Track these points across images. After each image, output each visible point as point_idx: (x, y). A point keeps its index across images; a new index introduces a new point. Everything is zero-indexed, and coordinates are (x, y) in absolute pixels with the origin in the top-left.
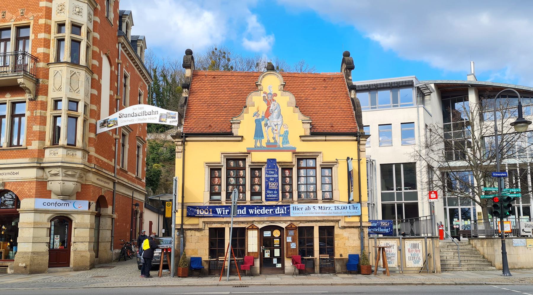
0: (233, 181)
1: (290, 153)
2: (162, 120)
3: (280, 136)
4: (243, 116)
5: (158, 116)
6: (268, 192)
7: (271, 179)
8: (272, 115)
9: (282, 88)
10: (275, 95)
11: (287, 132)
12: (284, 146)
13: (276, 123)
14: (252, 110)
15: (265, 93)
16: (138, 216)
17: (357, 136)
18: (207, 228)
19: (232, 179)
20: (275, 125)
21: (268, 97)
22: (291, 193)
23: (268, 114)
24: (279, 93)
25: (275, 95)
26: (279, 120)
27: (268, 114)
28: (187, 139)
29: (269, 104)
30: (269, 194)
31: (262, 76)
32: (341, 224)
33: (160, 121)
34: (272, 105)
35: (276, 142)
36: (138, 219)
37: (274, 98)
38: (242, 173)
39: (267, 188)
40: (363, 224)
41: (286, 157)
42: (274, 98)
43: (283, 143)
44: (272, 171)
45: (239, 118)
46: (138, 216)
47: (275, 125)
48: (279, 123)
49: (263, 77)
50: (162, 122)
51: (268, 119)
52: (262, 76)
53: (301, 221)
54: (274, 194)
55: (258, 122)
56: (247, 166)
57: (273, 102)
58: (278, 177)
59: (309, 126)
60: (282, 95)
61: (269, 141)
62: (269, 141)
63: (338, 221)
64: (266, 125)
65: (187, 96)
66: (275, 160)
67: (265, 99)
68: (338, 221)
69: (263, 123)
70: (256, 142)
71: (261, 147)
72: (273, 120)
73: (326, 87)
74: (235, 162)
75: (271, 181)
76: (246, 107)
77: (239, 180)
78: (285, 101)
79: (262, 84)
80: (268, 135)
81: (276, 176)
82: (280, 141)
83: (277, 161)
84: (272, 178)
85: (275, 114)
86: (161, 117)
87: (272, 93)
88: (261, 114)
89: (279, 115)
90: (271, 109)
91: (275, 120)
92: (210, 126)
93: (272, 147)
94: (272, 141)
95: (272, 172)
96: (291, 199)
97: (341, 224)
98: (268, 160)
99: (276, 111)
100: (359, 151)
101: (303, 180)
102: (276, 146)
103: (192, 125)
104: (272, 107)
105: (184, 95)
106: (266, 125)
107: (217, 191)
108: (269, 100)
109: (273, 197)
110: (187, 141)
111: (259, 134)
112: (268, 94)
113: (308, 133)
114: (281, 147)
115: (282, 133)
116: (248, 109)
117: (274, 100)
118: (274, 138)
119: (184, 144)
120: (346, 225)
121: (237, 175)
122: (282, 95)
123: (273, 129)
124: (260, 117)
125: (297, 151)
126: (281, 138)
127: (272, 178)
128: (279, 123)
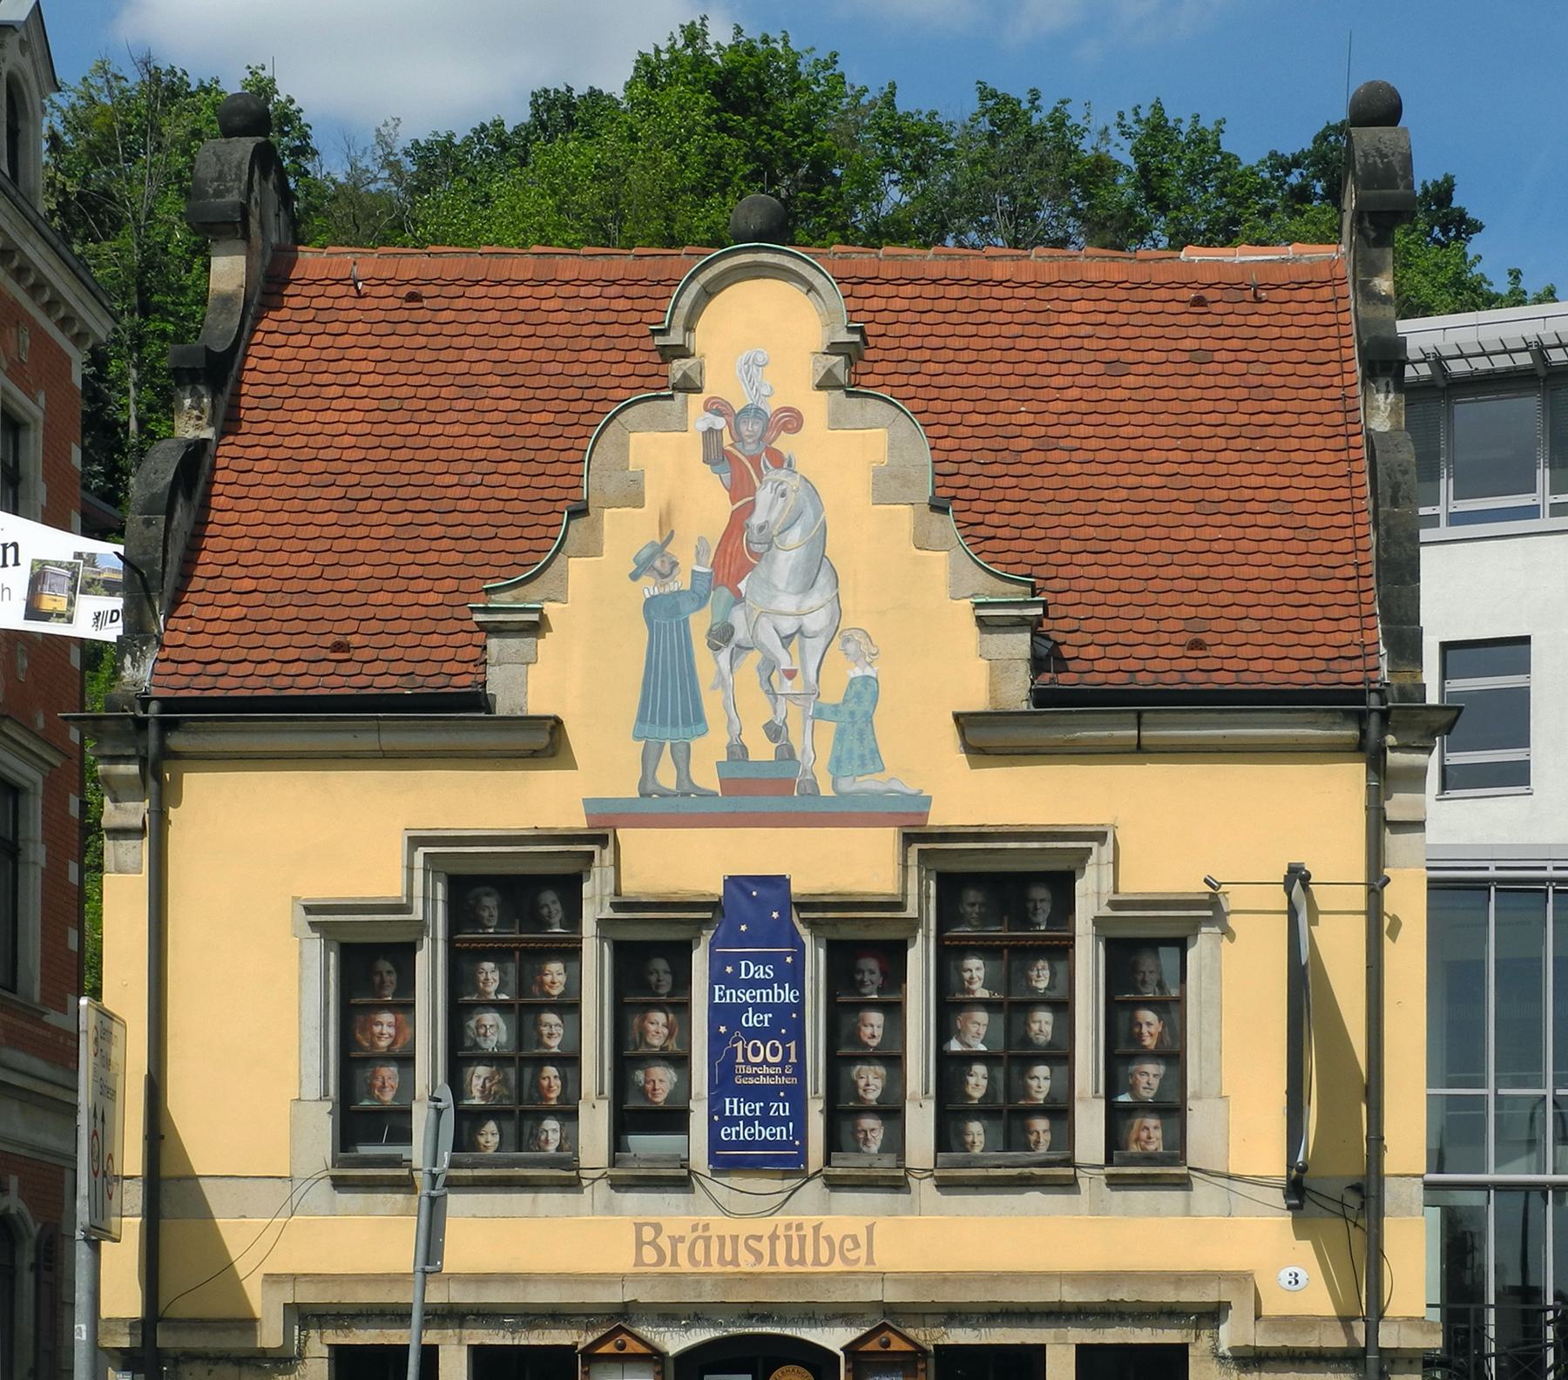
0: (494, 1030)
1: (888, 838)
2: (47, 604)
3: (819, 714)
4: (563, 578)
5: (18, 580)
6: (732, 1106)
7: (751, 1020)
8: (761, 569)
9: (842, 375)
10: (792, 420)
11: (865, 691)
12: (846, 785)
13: (788, 626)
14: (622, 531)
16: (27, 1257)
17: (1361, 718)
18: (318, 1345)
19: (490, 1018)
20: (786, 640)
21: (738, 438)
22: (891, 1112)
23: (735, 556)
24: (816, 406)
25: (792, 420)
26: (814, 599)
27: (735, 556)
28: (177, 741)
29: (741, 488)
30: (733, 1121)
31: (694, 288)
32: (1230, 1334)
33: (33, 612)
34: (764, 496)
35: (787, 754)
36: (27, 1281)
37: (784, 443)
38: (555, 972)
39: (723, 1082)
40: (1388, 1338)
41: (858, 864)
42: (784, 443)
43: (837, 764)
44: (758, 959)
45: (530, 595)
46: (27, 1257)
47: (786, 640)
49: (708, 293)
50: (45, 617)
51: (739, 598)
52: (694, 288)
53: (955, 1315)
54: (766, 1120)
55: (664, 616)
56: (589, 927)
57: (773, 475)
58: (799, 1007)
59: (1021, 643)
60: (836, 423)
61: (737, 752)
62: (737, 752)
63: (1213, 1315)
64: (722, 636)
65: (209, 434)
66: (780, 882)
67: (715, 455)
68: (1213, 1315)
69: (700, 623)
70: (649, 761)
71: (687, 789)
72: (778, 596)
73: (1201, 358)
74: (508, 902)
75: (751, 1034)
76: (579, 511)
77: (537, 1024)
78: (853, 462)
79: (700, 340)
80: (736, 711)
81: (788, 996)
82: (816, 749)
83: (799, 887)
84: (760, 1008)
85: (786, 560)
86: (38, 580)
87: (771, 406)
88: (690, 562)
89: (818, 565)
90: (756, 520)
91: (787, 602)
92: (338, 647)
93: (763, 793)
94: (762, 750)
95: (761, 972)
96: (889, 1160)
97: (1230, 1334)
98: (733, 882)
99: (794, 535)
100: (1379, 824)
101: (977, 1030)
102: (783, 786)
103: (219, 638)
104: (766, 507)
105: (190, 426)
107: (388, 1097)
109: (765, 1145)
110: (178, 756)
111: (669, 702)
112: (736, 419)
113: (1016, 694)
114: (826, 790)
115: (833, 693)
116: (596, 529)
117: (778, 460)
118: (774, 731)
119: (159, 778)
120: (1263, 1339)
121: (522, 989)
122: (836, 423)
123: (769, 665)
124: (682, 581)
125: (938, 818)
126: (827, 730)
127: (760, 1008)
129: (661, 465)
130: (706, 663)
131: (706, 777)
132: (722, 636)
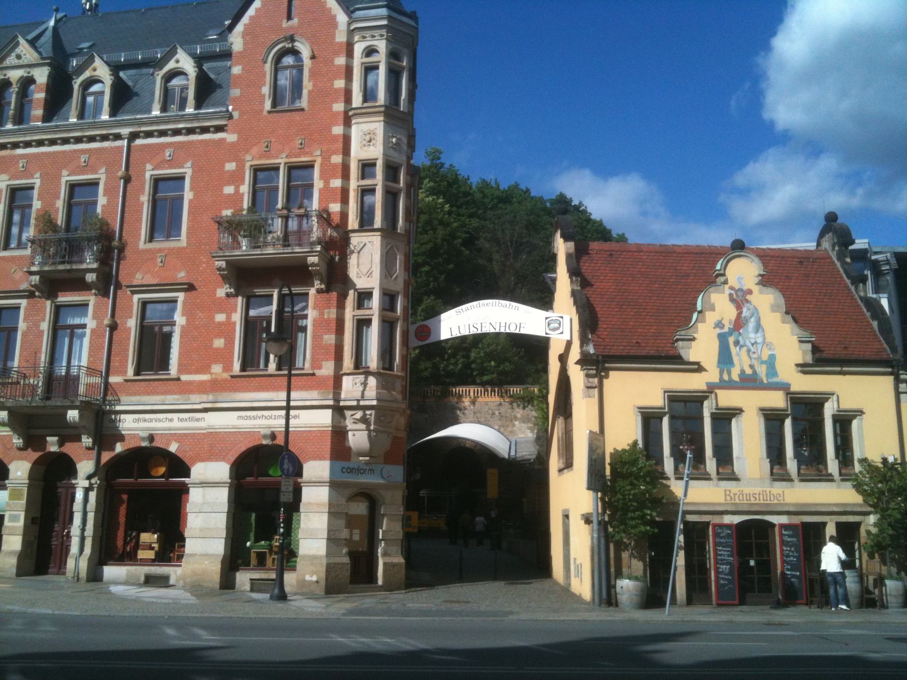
10: (750, 292)
11: (772, 357)
12: (770, 380)
15: (732, 288)
23: (739, 324)
24: (756, 289)
25: (750, 292)
27: (739, 324)
29: (739, 307)
48: (760, 340)
67: (732, 299)
69: (731, 340)
72: (750, 334)
80: (741, 362)
82: (762, 370)
85: (751, 325)
89: (758, 327)
94: (749, 371)
104: (745, 312)
106: (737, 343)
108: (739, 299)
111: (725, 358)
118: (751, 367)
124: (726, 330)
128: (760, 340)
129: (718, 306)
130: (734, 350)
131: (735, 377)
132: (737, 343)
